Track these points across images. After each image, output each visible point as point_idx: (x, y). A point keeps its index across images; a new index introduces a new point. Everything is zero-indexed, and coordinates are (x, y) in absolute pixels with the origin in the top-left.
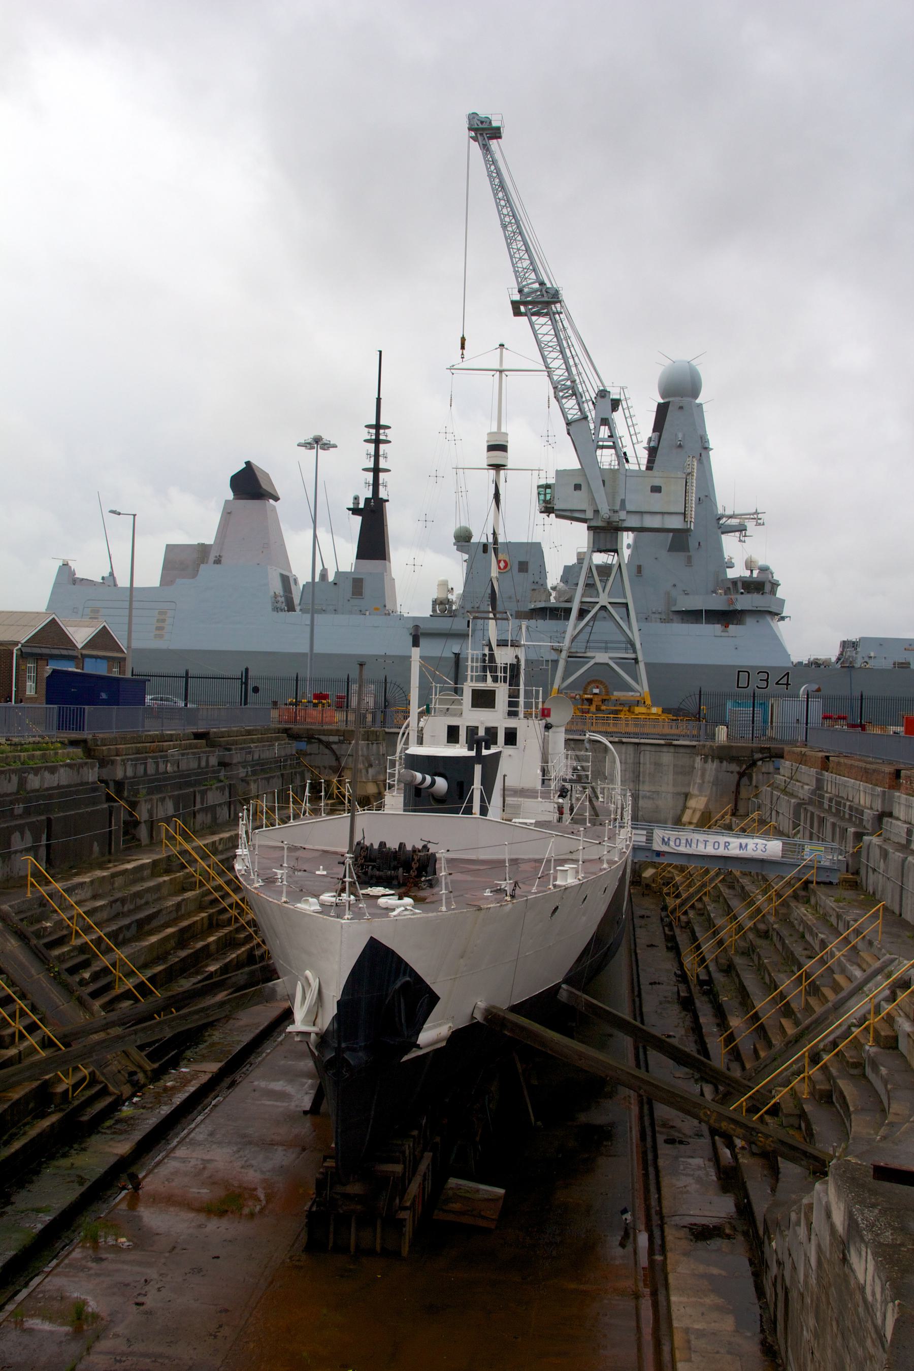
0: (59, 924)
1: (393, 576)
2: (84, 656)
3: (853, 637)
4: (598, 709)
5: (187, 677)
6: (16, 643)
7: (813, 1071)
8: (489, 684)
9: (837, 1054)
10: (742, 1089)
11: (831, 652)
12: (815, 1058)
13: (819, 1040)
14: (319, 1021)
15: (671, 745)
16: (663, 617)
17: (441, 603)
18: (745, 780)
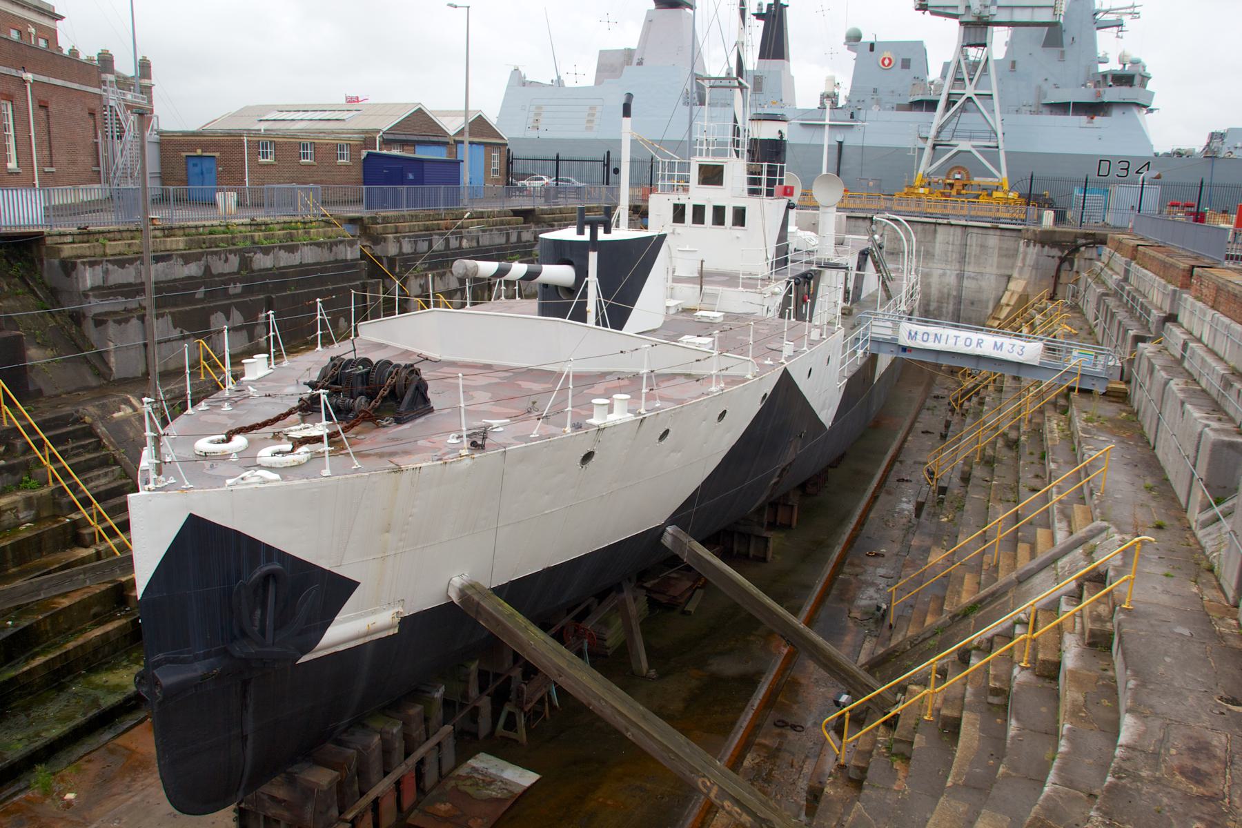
1: (792, 73)
3: (1221, 129)
4: (959, 193)
5: (558, 160)
6: (378, 131)
10: (859, 688)
11: (1197, 143)
15: (997, 228)
16: (1033, 109)
17: (828, 97)
18: (1066, 265)
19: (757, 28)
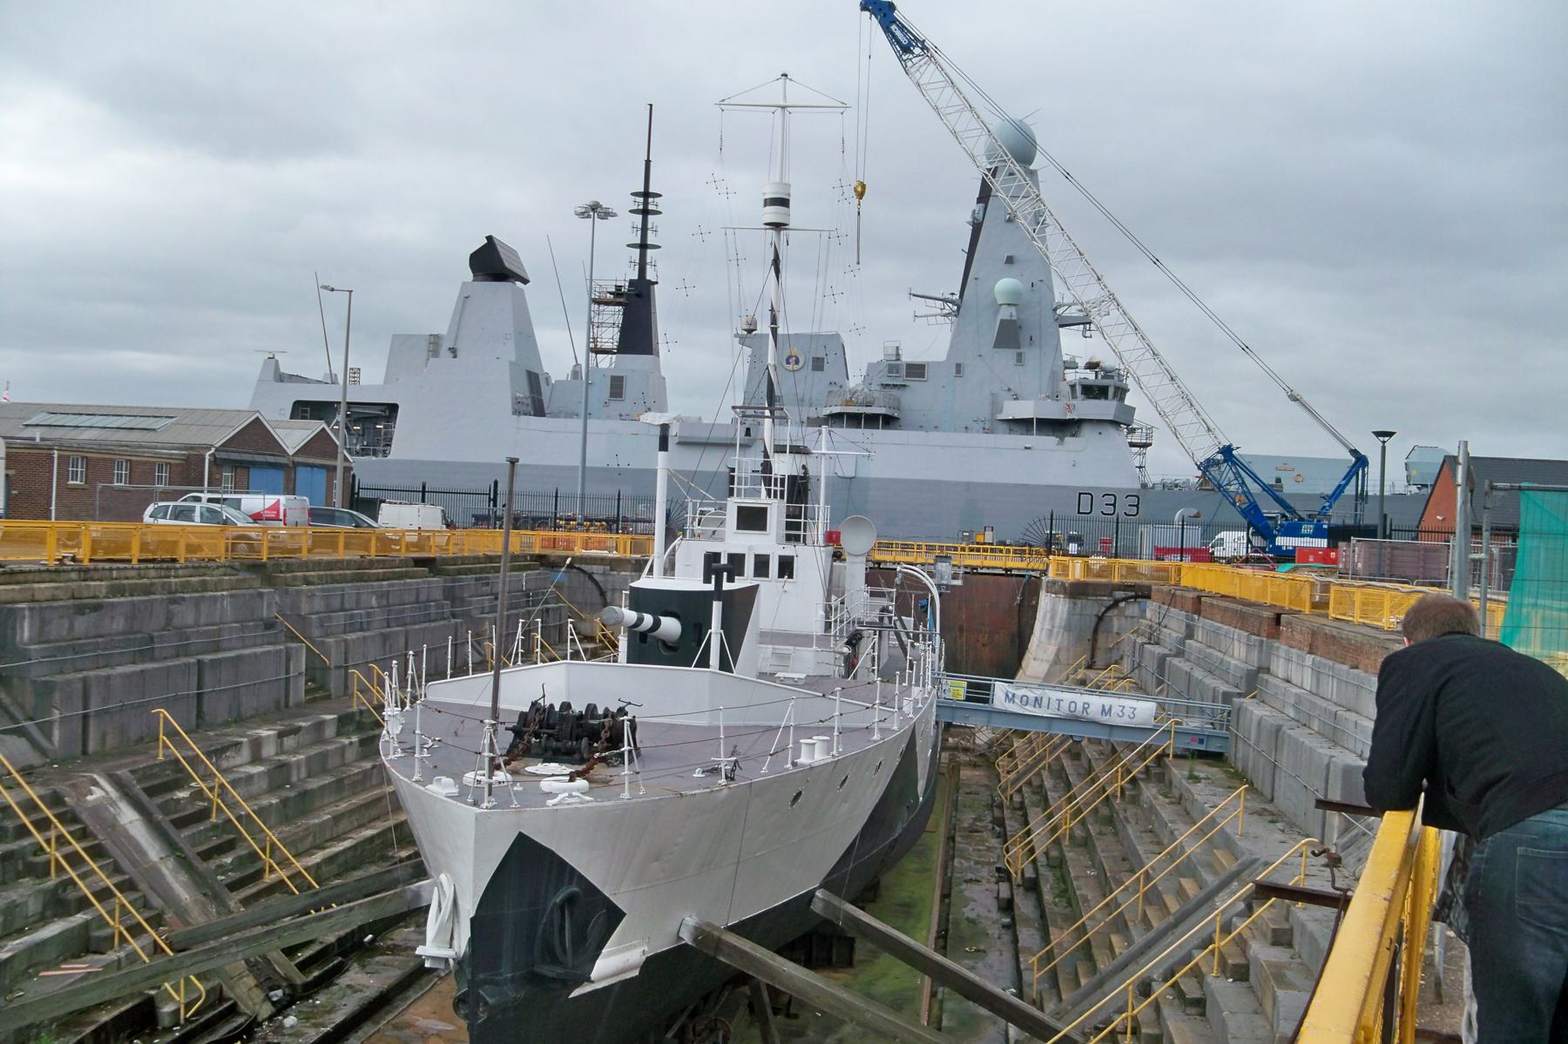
0: (198, 794)
2: (296, 465)
6: (208, 448)
7: (1142, 1008)
8: (762, 500)
9: (1173, 986)
12: (1145, 989)
13: (1150, 966)
14: (455, 942)
19: (614, 315)
